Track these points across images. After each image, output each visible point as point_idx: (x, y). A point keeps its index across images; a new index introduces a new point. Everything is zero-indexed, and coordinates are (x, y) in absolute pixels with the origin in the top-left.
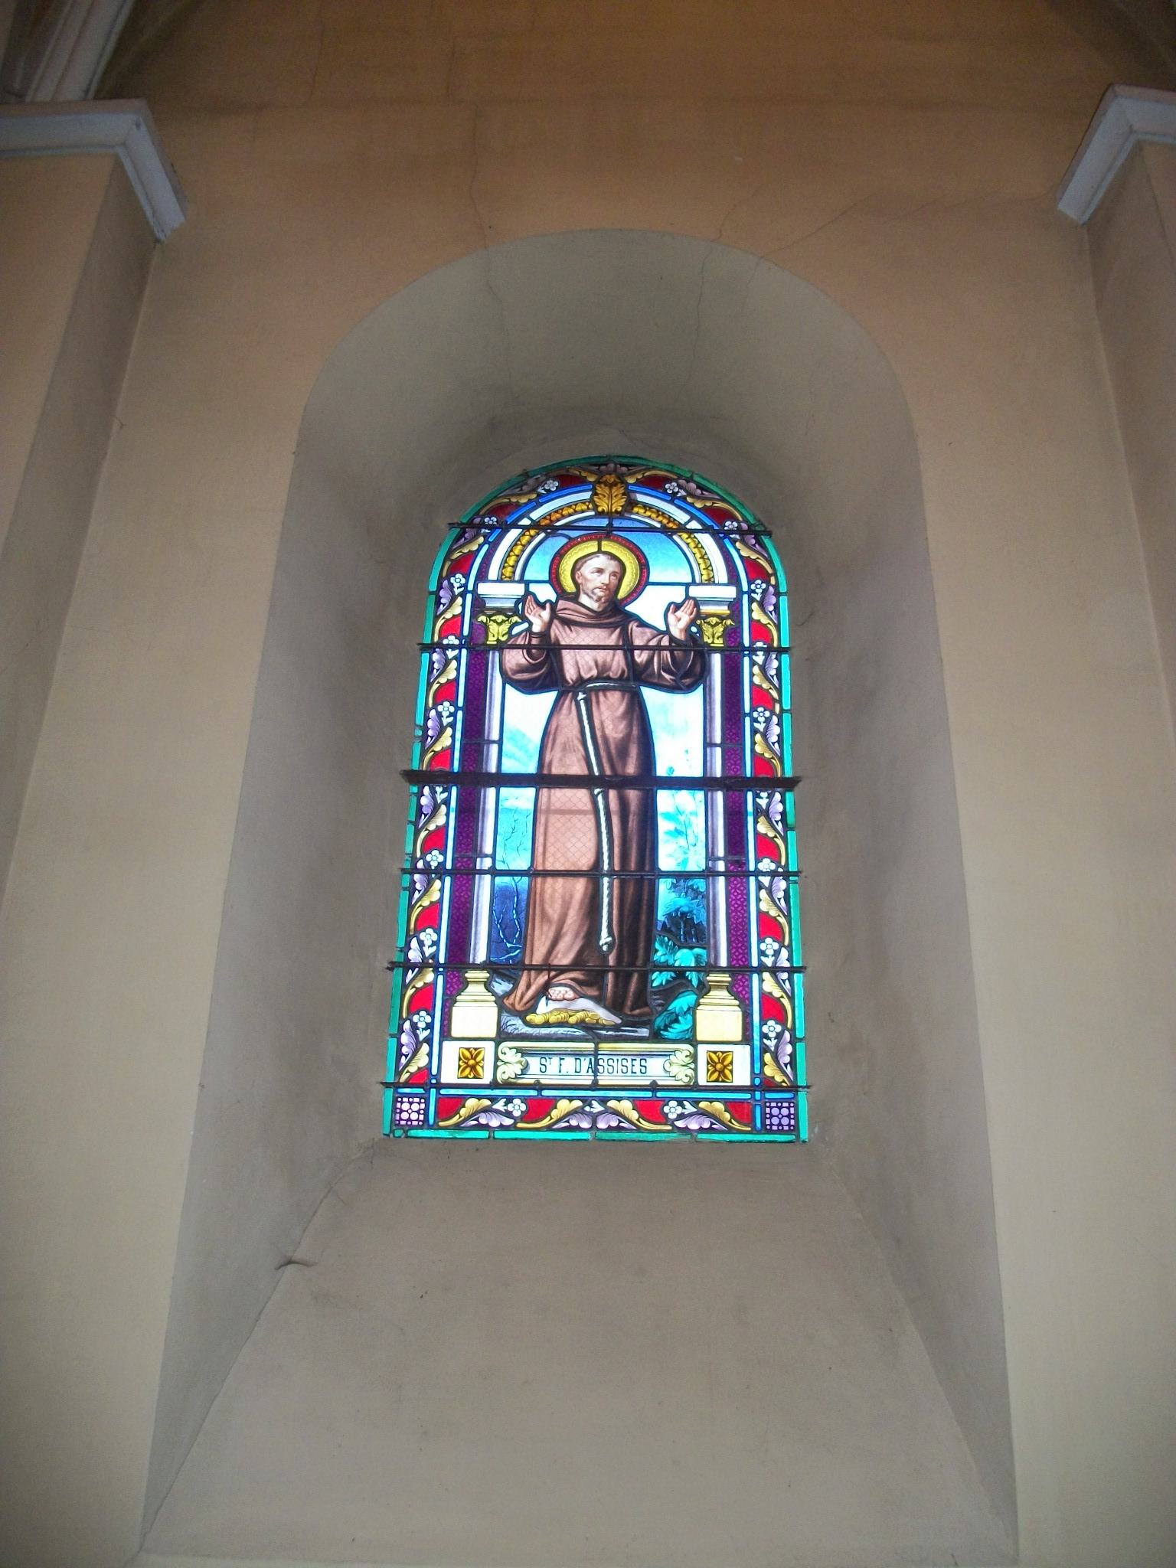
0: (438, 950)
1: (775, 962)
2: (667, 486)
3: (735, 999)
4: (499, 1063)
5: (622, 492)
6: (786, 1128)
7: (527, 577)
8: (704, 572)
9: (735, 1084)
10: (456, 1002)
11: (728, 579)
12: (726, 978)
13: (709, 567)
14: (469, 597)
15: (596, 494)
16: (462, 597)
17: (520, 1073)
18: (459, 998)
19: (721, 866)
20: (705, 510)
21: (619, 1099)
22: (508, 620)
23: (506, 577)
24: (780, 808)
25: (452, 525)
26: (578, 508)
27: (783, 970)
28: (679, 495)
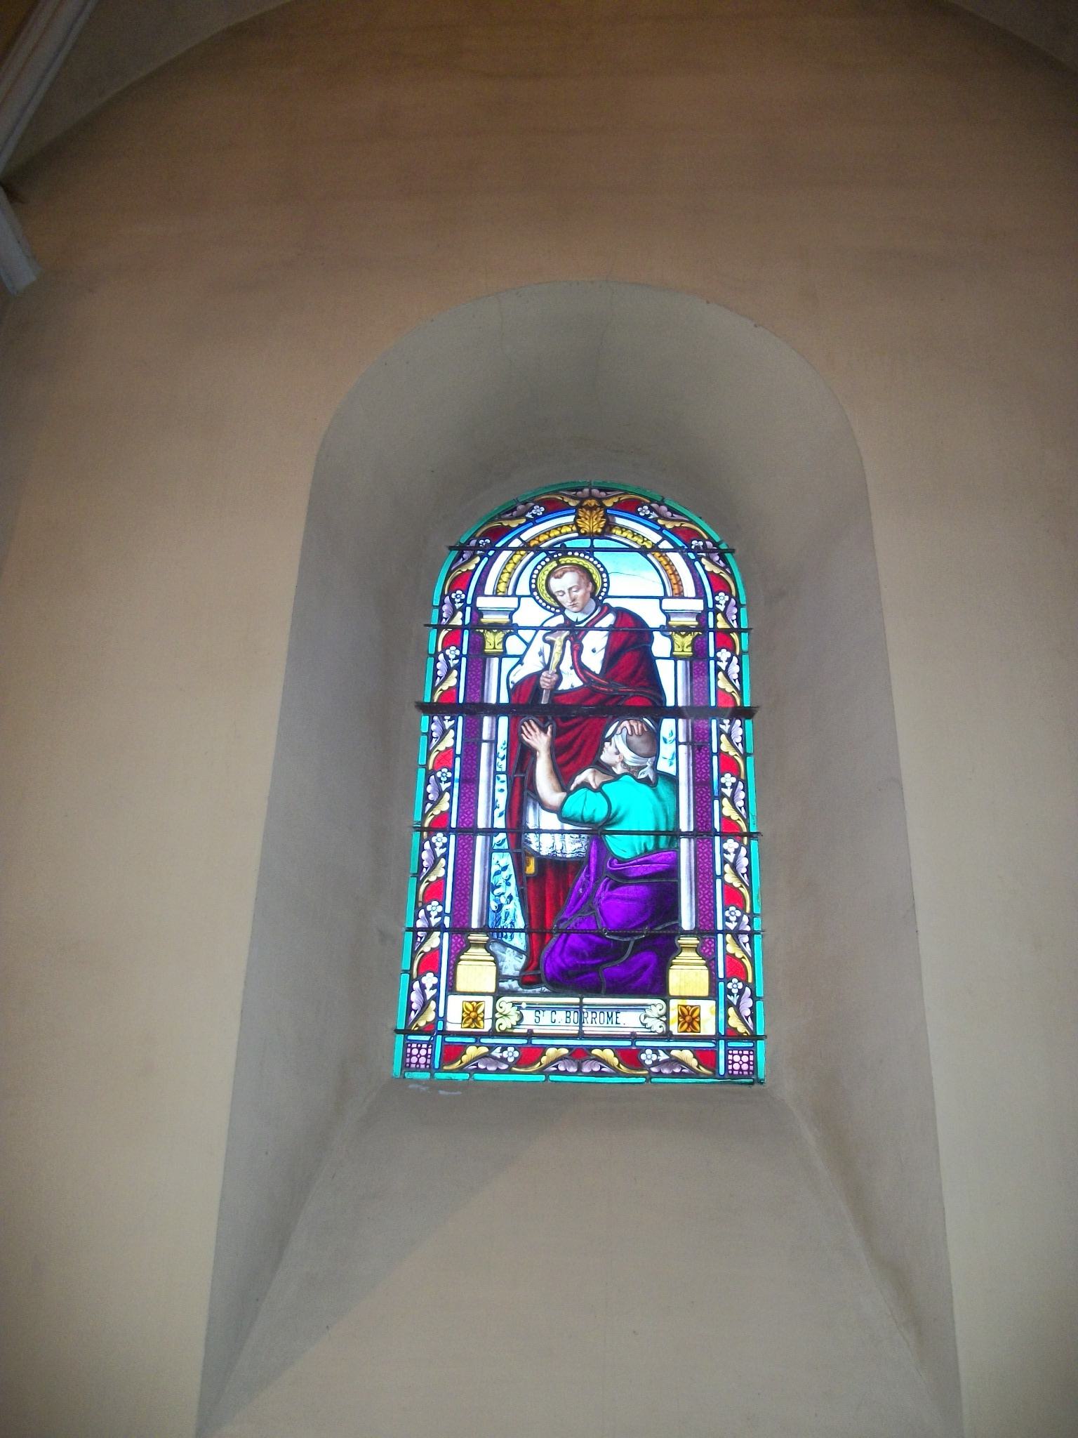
0: (448, 850)
3: (703, 959)
4: (497, 1015)
6: (746, 1073)
7: (518, 593)
9: (702, 1033)
11: (709, 992)
12: (693, 941)
13: (679, 583)
14: (468, 609)
15: (579, 517)
16: (445, 858)
17: (515, 1024)
18: (462, 957)
20: (674, 531)
21: (602, 1048)
25: (451, 548)
26: (563, 531)
27: (745, 933)
28: (651, 517)
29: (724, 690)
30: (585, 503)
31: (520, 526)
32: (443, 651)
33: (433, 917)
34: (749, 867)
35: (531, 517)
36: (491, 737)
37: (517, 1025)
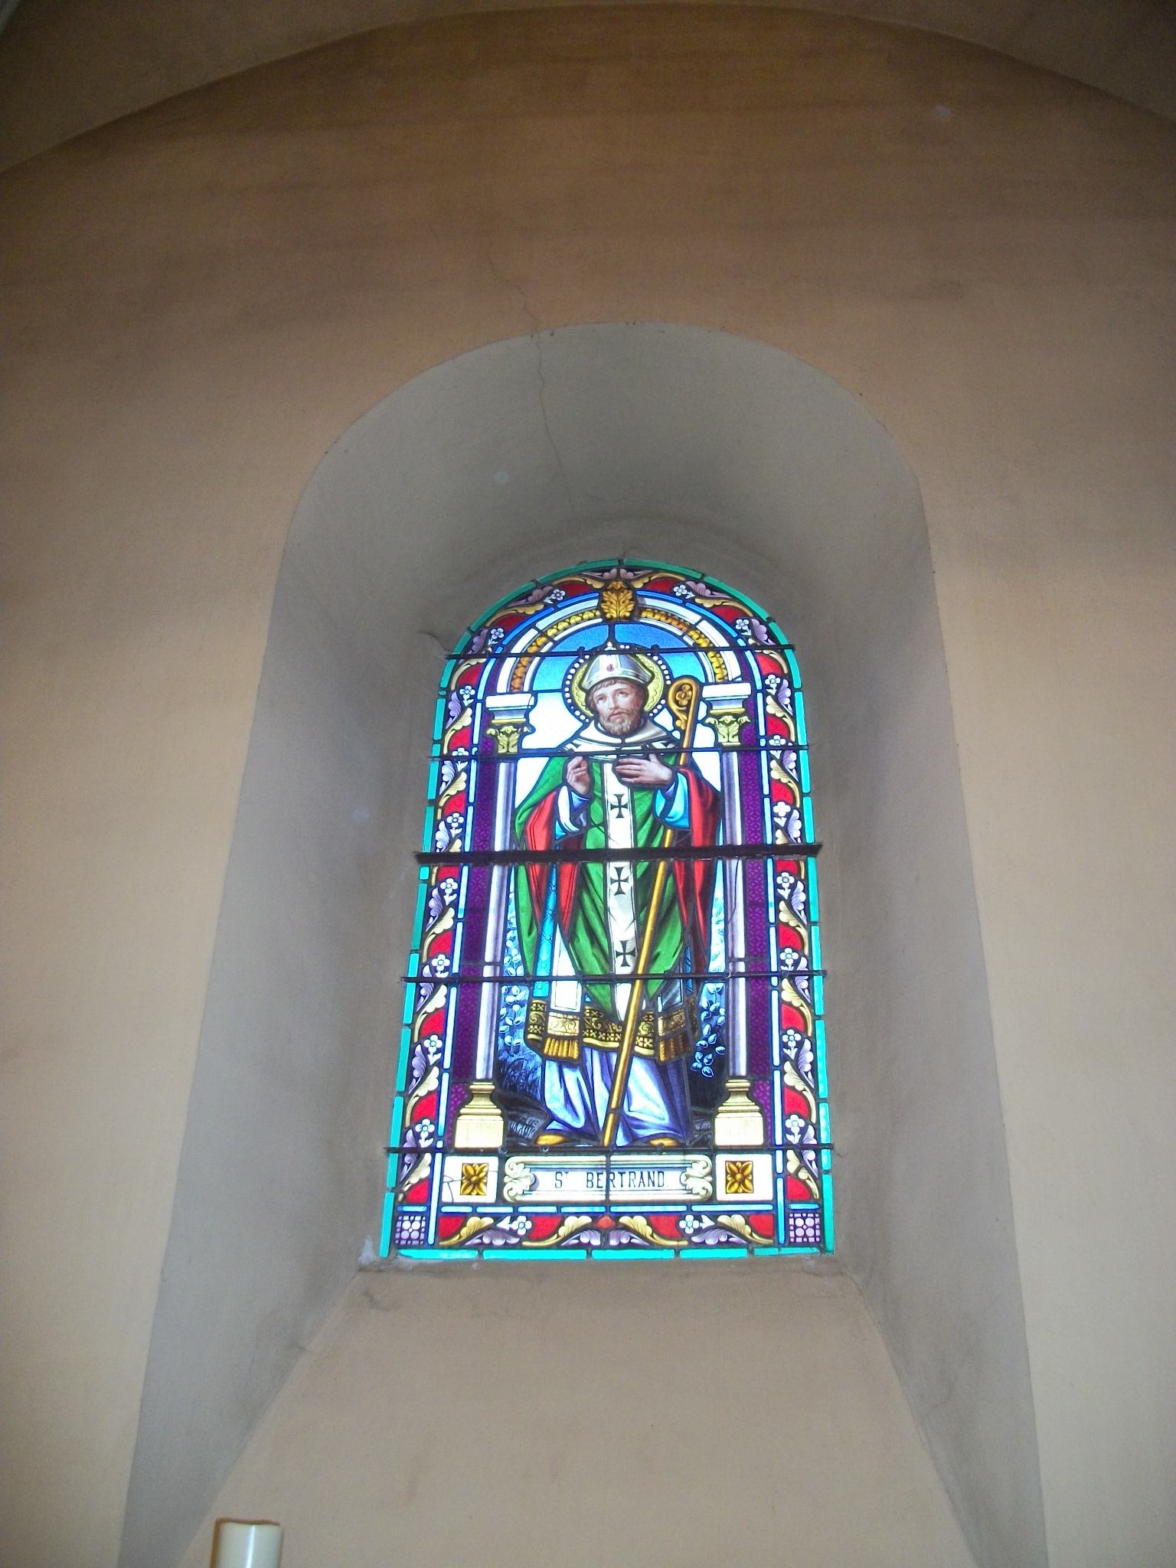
1: (801, 1139)
2: (675, 589)
3: (756, 1105)
5: (630, 597)
8: (717, 671)
10: (460, 1115)
15: (604, 602)
18: (463, 1111)
19: (741, 967)
22: (517, 731)
23: (515, 688)
24: (802, 897)
27: (809, 1147)
28: (688, 597)
29: (774, 715)
30: (611, 586)
31: (537, 612)
32: (457, 690)
33: (423, 1139)
34: (814, 1064)
35: (550, 602)
36: (495, 956)
37: (530, 1190)
